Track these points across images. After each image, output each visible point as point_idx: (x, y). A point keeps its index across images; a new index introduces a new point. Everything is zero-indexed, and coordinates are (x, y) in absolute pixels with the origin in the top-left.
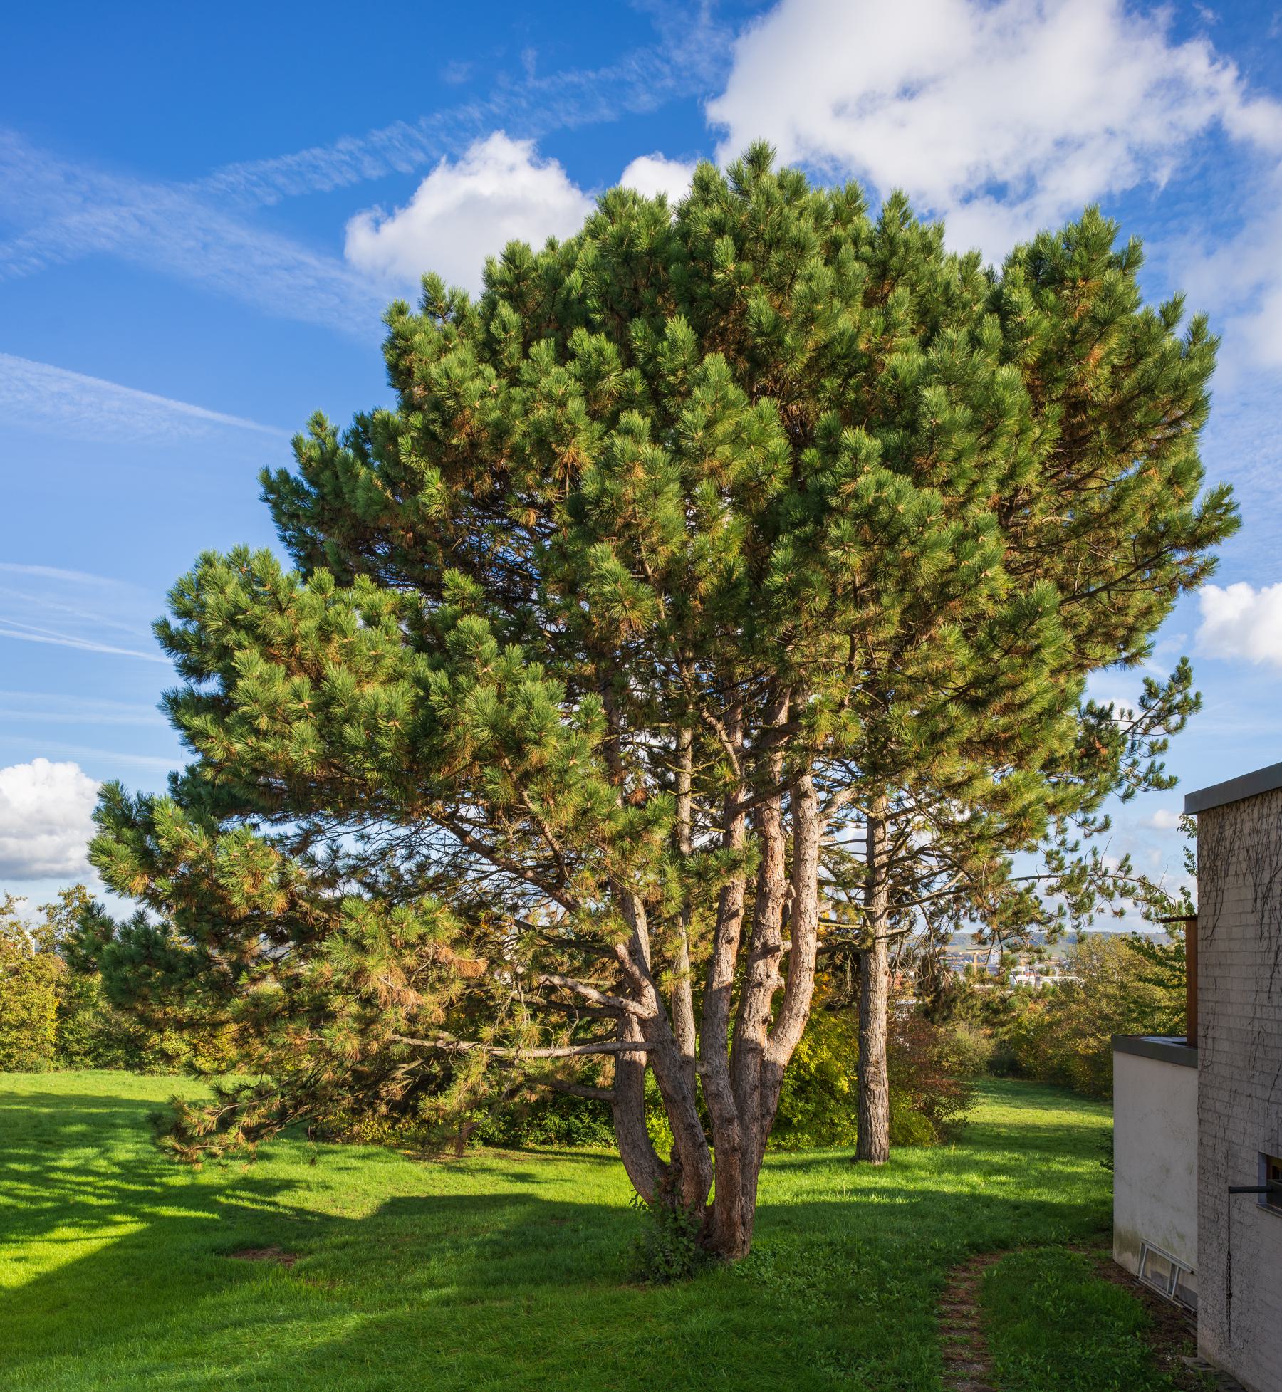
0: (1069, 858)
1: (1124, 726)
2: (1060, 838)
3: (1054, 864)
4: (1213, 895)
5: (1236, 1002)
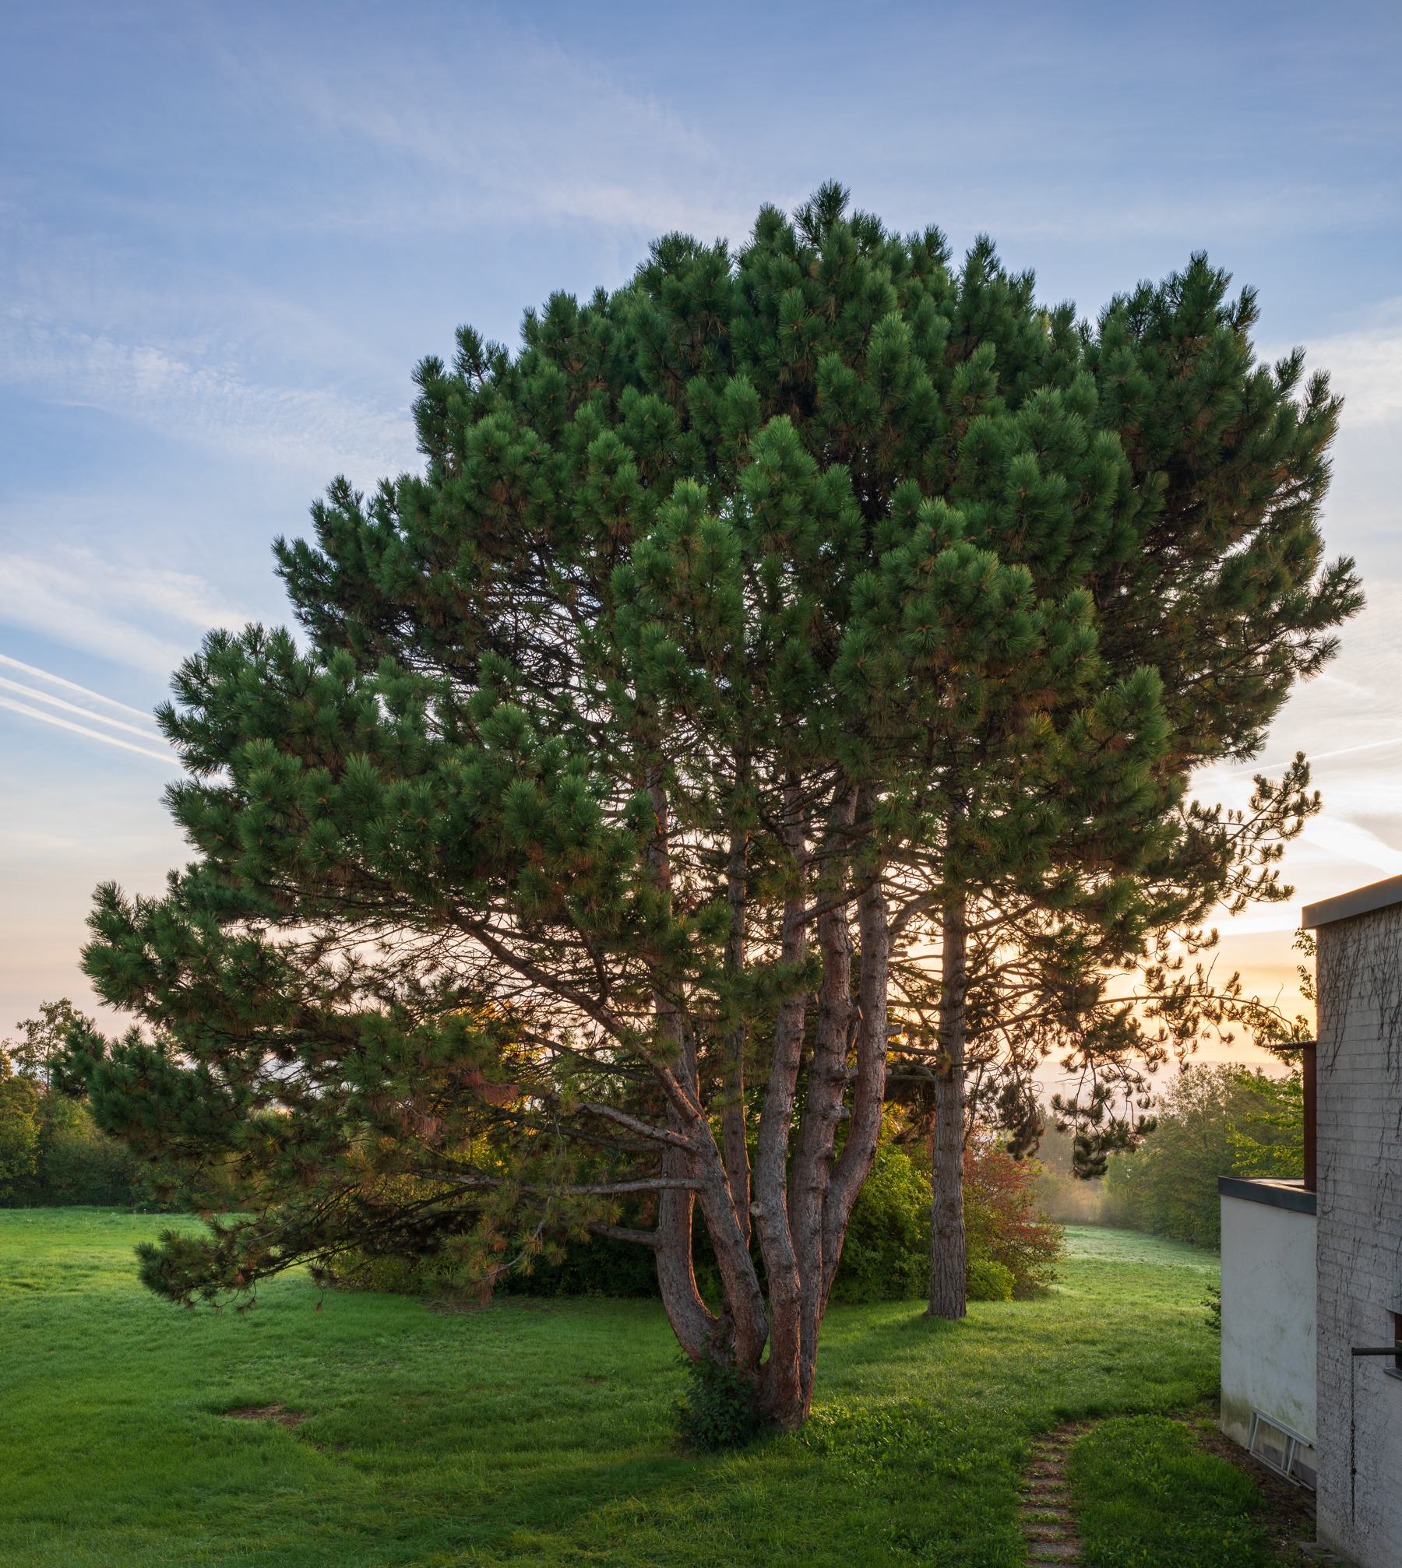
0: (1170, 977)
1: (1232, 830)
2: (1161, 953)
3: (1156, 982)
4: (1334, 1020)
5: (1359, 1140)
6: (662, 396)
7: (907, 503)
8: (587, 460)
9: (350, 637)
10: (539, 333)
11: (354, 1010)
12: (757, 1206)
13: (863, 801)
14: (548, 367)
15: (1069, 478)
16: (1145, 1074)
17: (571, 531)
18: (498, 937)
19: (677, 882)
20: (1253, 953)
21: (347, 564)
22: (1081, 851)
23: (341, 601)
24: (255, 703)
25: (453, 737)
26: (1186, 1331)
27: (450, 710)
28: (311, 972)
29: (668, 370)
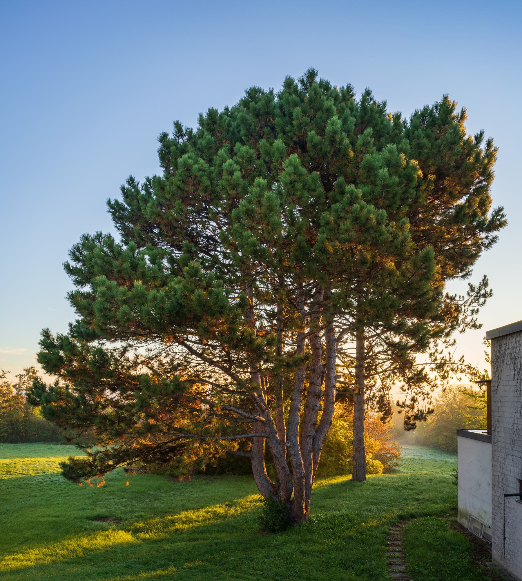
0: (439, 356)
1: (460, 303)
2: (435, 348)
3: (433, 358)
4: (497, 373)
5: (507, 416)
6: (250, 145)
8: (222, 170)
10: (204, 122)
11: (138, 373)
12: (288, 443)
13: (326, 293)
14: (208, 136)
15: (399, 177)
16: (430, 392)
17: (217, 196)
18: (191, 344)
19: (258, 324)
20: (468, 350)
21: (134, 208)
22: (407, 311)
23: (132, 222)
24: (100, 262)
25: (174, 273)
26: (445, 484)
27: (172, 261)
28: (122, 360)
29: (253, 137)
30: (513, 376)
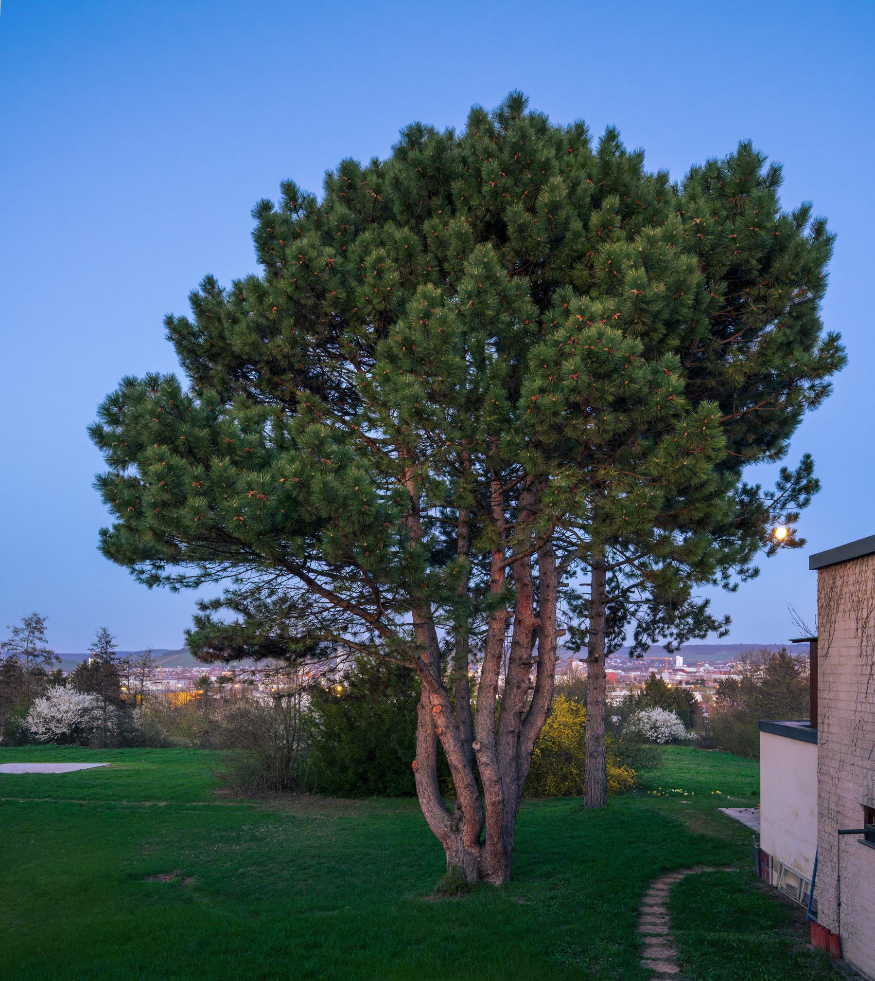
1: (768, 503)
4: (828, 625)
7: (564, 300)
9: (215, 381)
14: (341, 209)
18: (312, 576)
25: (282, 446)
30: (855, 630)
